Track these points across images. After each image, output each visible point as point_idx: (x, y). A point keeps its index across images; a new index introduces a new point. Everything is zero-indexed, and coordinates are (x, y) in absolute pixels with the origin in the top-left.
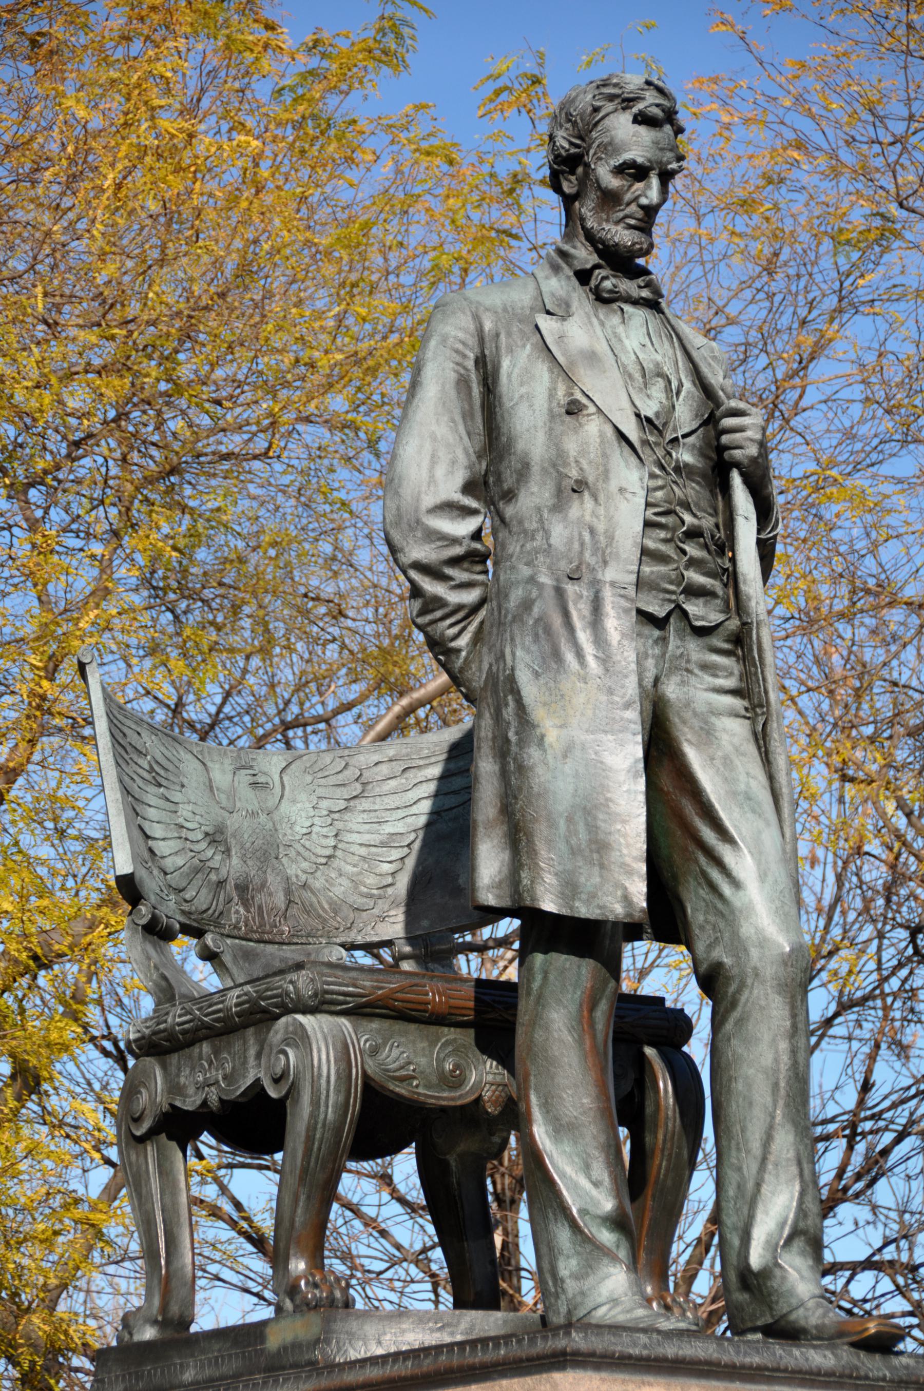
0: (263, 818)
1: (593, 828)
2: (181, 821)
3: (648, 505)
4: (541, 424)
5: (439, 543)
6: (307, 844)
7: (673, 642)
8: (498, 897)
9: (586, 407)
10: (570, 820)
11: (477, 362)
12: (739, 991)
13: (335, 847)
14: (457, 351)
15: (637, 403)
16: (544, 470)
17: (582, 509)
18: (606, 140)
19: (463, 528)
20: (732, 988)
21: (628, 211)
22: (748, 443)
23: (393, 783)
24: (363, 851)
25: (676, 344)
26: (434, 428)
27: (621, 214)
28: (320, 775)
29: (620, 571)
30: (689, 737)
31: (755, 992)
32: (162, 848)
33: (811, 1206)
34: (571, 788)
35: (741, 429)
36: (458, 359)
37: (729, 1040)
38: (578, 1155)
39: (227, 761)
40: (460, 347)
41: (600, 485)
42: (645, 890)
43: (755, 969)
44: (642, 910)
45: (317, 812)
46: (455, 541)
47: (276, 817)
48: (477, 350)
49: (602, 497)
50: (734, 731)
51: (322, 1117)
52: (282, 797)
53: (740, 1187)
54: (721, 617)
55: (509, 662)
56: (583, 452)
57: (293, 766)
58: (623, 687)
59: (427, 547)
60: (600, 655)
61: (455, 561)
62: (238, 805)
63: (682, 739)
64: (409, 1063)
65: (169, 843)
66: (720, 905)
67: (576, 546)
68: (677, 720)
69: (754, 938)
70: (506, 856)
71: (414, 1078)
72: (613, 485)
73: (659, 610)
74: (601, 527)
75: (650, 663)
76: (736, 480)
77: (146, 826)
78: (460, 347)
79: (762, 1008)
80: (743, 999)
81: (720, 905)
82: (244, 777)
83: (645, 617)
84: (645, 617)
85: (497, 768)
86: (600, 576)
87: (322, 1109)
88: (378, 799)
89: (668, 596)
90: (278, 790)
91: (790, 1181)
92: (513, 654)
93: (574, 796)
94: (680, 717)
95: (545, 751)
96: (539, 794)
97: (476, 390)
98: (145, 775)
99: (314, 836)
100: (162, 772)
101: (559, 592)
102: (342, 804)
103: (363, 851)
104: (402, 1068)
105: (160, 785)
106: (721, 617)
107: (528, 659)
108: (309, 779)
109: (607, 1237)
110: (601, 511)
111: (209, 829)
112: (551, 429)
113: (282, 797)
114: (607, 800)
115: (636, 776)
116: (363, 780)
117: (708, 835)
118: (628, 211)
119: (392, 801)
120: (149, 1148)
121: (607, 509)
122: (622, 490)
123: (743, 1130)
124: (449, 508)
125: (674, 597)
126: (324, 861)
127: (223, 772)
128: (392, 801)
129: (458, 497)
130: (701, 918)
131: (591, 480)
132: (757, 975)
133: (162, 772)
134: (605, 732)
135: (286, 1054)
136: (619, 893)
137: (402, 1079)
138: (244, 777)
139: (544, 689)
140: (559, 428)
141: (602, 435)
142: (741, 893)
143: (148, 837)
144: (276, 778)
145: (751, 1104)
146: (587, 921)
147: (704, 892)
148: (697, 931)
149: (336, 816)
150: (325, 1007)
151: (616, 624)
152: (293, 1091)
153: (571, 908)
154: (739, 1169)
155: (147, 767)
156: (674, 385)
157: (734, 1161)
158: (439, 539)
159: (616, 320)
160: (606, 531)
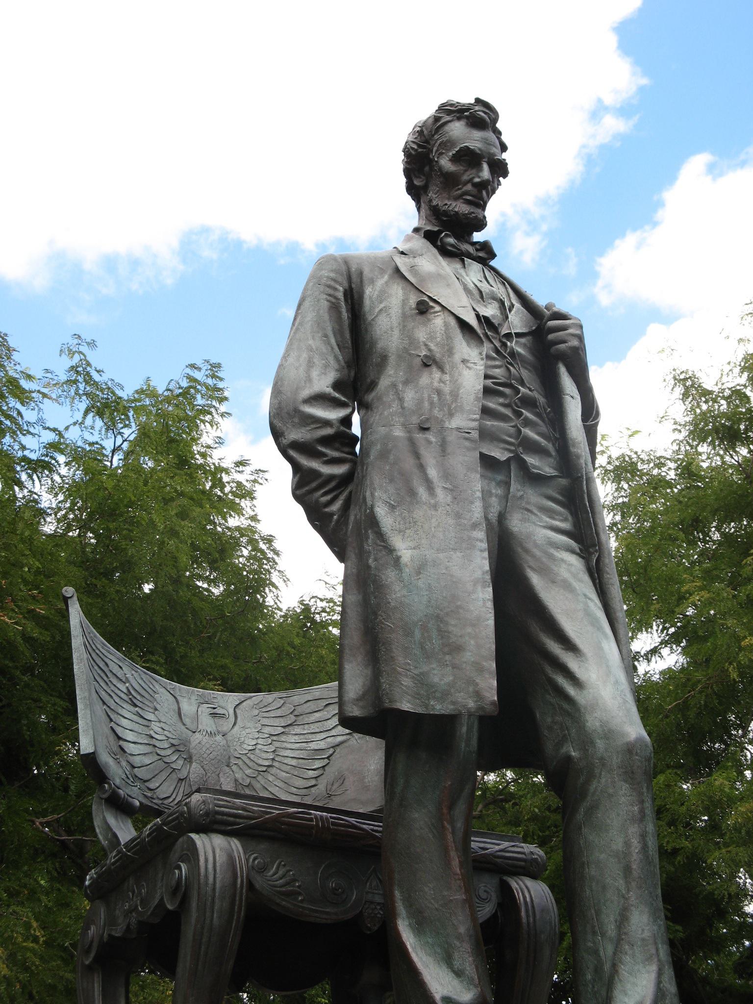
0: (219, 738)
1: (443, 634)
2: (152, 733)
3: (487, 377)
4: (395, 324)
5: (313, 426)
6: (252, 757)
7: (514, 486)
8: (363, 707)
9: (432, 307)
10: (424, 628)
11: (345, 294)
12: (588, 782)
13: (273, 759)
14: (329, 286)
15: (478, 310)
16: (399, 357)
17: (431, 379)
18: (445, 139)
19: (334, 415)
20: (582, 779)
21: (465, 188)
22: (570, 338)
23: (317, 715)
24: (294, 762)
25: (508, 286)
26: (311, 342)
27: (459, 192)
28: (264, 710)
29: (466, 419)
31: (603, 780)
32: (130, 748)
33: (667, 985)
34: (425, 599)
36: (331, 292)
37: (580, 828)
39: (194, 698)
40: (332, 283)
41: (445, 360)
42: (495, 683)
43: (602, 759)
44: (493, 703)
45: (261, 735)
46: (327, 423)
47: (229, 737)
48: (346, 285)
49: (447, 367)
50: (571, 565)
51: (208, 921)
52: (235, 724)
53: (598, 970)
54: (553, 473)
55: (369, 503)
56: (432, 337)
57: (244, 704)
58: (470, 511)
59: (303, 430)
60: (448, 486)
61: (326, 441)
62: (200, 727)
63: (525, 566)
64: (295, 880)
65: (139, 746)
66: (566, 706)
67: (426, 404)
68: (520, 550)
69: (600, 730)
70: (369, 672)
71: (300, 894)
72: (457, 358)
73: (501, 455)
74: (447, 389)
75: (494, 501)
77: (119, 730)
78: (332, 283)
79: (610, 796)
80: (592, 789)
81: (566, 706)
83: (487, 462)
84: (487, 462)
85: (360, 597)
86: (447, 425)
87: (208, 914)
88: (306, 726)
89: (508, 447)
90: (232, 719)
91: (648, 959)
92: (372, 495)
93: (427, 607)
95: (401, 570)
96: (395, 608)
97: (345, 315)
98: (123, 695)
99: (257, 751)
100: (138, 697)
101: (412, 442)
102: (281, 730)
103: (294, 762)
104: (287, 884)
105: (135, 706)
106: (553, 473)
107: (385, 496)
108: (256, 712)
110: (447, 377)
111: (174, 742)
112: (404, 326)
113: (235, 724)
114: (458, 607)
116: (296, 713)
117: (555, 648)
118: (465, 188)
119: (314, 728)
120: (96, 979)
121: (452, 376)
122: (464, 361)
123: (598, 913)
124: (319, 398)
125: (513, 448)
126: (264, 769)
127: (190, 704)
128: (314, 728)
129: (329, 390)
130: (549, 720)
131: (438, 356)
132: (603, 765)
133: (138, 697)
134: (454, 550)
135: (179, 868)
136: (471, 689)
137: (288, 894)
138: (205, 709)
139: (399, 519)
140: (410, 325)
141: (446, 325)
142: (585, 692)
143: (119, 738)
144: (231, 711)
145: (604, 888)
146: (443, 716)
147: (552, 699)
148: (546, 733)
149: (274, 738)
150: (216, 827)
151: (464, 460)
152: (184, 901)
153: (426, 706)
154: (596, 952)
155: (125, 690)
156: (507, 304)
157: (590, 944)
158: (313, 423)
159: (458, 266)
160: (451, 392)
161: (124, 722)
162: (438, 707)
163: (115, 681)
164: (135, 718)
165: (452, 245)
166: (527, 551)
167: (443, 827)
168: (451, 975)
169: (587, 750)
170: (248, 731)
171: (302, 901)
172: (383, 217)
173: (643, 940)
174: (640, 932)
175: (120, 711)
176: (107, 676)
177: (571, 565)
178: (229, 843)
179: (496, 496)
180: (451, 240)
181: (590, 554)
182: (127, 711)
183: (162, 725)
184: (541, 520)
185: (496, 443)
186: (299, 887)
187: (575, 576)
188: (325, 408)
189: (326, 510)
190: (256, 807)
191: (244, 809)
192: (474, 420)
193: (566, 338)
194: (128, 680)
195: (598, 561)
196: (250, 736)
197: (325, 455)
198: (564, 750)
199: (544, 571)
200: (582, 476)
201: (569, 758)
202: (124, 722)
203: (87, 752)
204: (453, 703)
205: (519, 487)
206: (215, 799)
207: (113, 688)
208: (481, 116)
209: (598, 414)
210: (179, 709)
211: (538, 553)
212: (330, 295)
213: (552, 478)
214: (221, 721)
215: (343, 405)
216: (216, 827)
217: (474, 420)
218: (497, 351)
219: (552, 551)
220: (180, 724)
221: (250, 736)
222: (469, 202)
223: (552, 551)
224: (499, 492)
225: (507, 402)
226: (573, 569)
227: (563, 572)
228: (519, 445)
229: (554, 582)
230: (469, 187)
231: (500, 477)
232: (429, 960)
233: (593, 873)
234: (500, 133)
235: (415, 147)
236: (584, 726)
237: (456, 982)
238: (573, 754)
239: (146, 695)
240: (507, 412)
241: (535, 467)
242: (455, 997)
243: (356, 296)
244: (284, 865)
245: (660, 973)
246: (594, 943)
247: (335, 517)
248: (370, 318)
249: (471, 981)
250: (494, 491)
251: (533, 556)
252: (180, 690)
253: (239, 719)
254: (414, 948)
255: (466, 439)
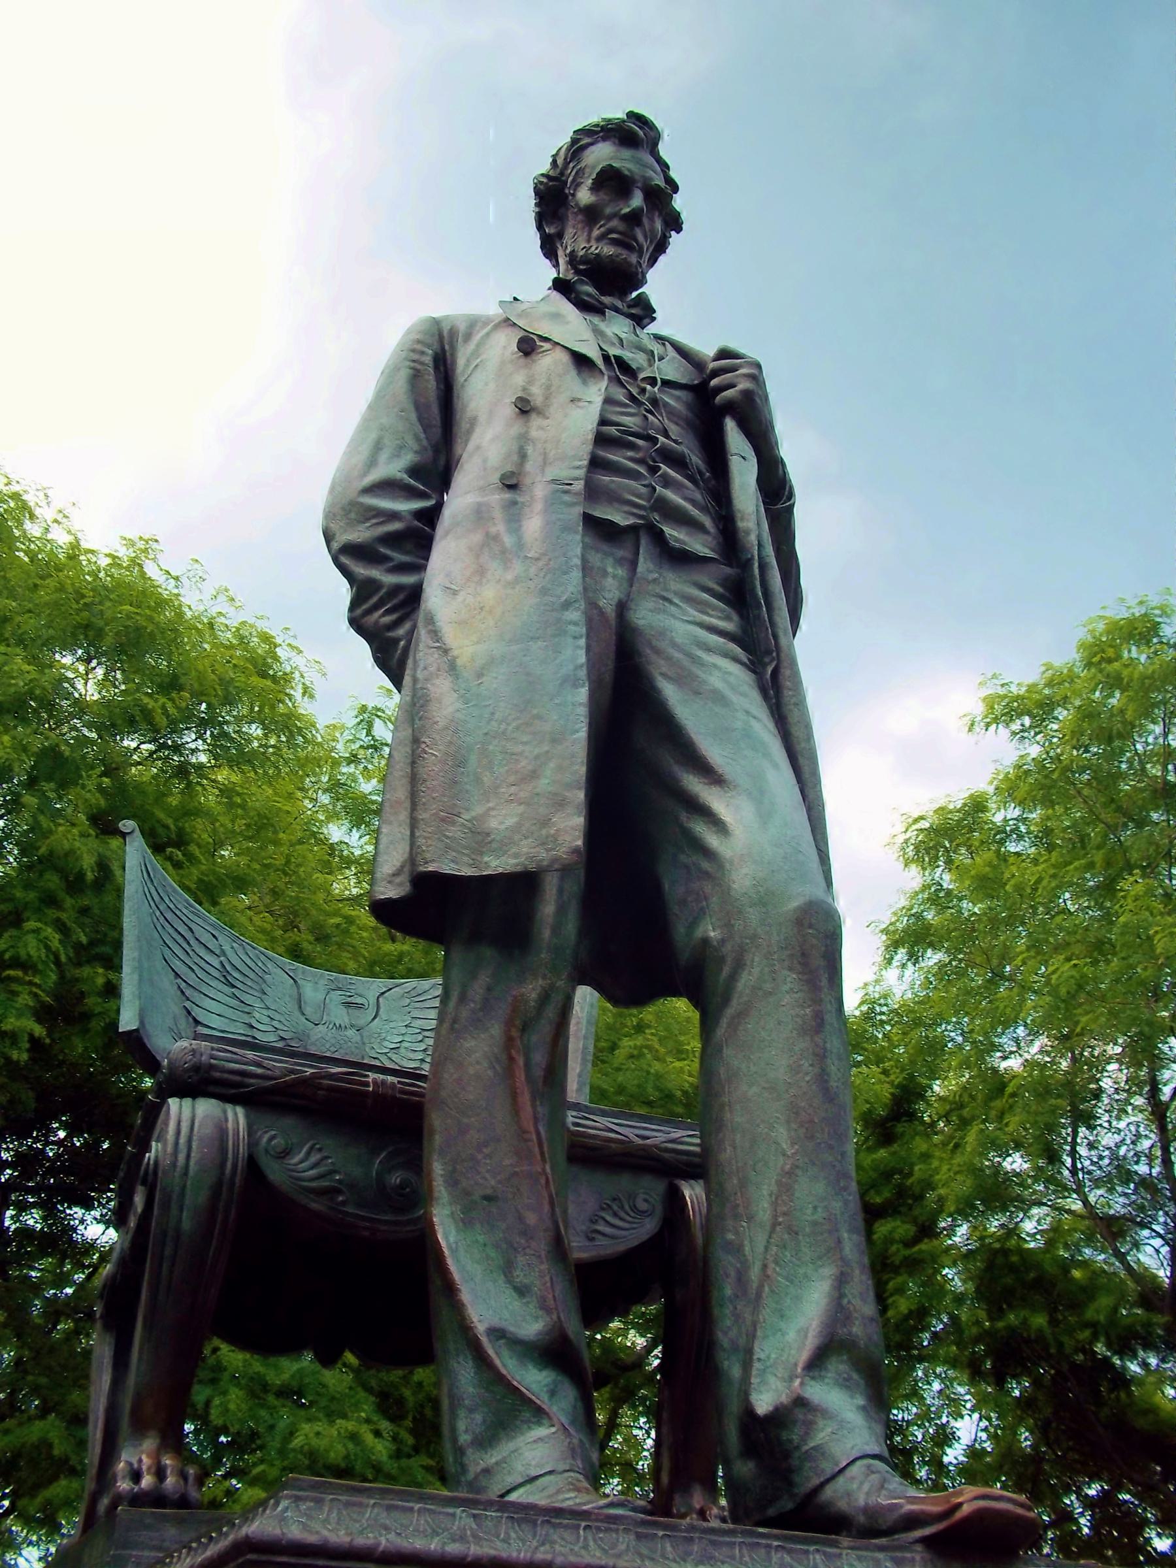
6: (394, 1057)
12: (733, 977)
20: (726, 971)
30: (664, 670)
33: (857, 1302)
35: (733, 369)
37: (720, 1051)
38: (497, 1246)
45: (410, 1030)
46: (394, 516)
48: (436, 346)
54: (711, 554)
59: (361, 527)
61: (391, 539)
73: (620, 518)
76: (730, 425)
77: (197, 1013)
81: (824, 982)
82: (336, 996)
89: (635, 511)
94: (653, 648)
98: (216, 974)
99: (402, 1050)
104: (321, 1177)
105: (234, 986)
109: (534, 1380)
115: (576, 685)
123: (743, 1184)
125: (642, 513)
127: (316, 990)
144: (373, 1001)
148: (676, 909)
150: (211, 1089)
157: (730, 1236)
158: (374, 517)
161: (207, 1003)
162: (494, 864)
163: (202, 952)
164: (234, 1002)
165: (589, 295)
166: (658, 652)
167: (511, 1059)
168: (510, 1292)
169: (733, 926)
170: (392, 1025)
171: (343, 1203)
172: (507, 274)
173: (815, 1224)
174: (809, 1211)
175: (205, 989)
176: (188, 943)
177: (730, 673)
178: (225, 1112)
179: (614, 577)
180: (589, 289)
181: (765, 665)
182: (217, 990)
183: (270, 1013)
184: (685, 613)
185: (616, 505)
186: (339, 1181)
187: (733, 688)
188: (394, 498)
189: (390, 634)
190: (278, 1065)
191: (259, 1065)
192: (578, 468)
193: (736, 380)
194: (224, 953)
195: (775, 672)
196: (395, 1032)
197: (387, 559)
198: (699, 933)
199: (684, 679)
200: (752, 558)
201: (706, 941)
202: (207, 1003)
203: (129, 1028)
204: (516, 856)
205: (651, 566)
206: (213, 1049)
207: (197, 960)
208: (634, 133)
209: (791, 495)
210: (300, 995)
211: (677, 655)
212: (414, 361)
213: (705, 560)
214: (356, 1012)
215: (422, 495)
216: (211, 1089)
217: (578, 468)
218: (632, 398)
219: (700, 653)
220: (297, 1013)
221: (395, 1032)
222: (615, 242)
223: (700, 653)
224: (621, 572)
225: (639, 455)
226: (732, 679)
227: (715, 681)
228: (654, 508)
229: (697, 693)
230: (614, 223)
231: (620, 553)
232: (477, 1270)
233: (738, 1119)
234: (668, 168)
235: (545, 180)
236: (729, 888)
237: (516, 1304)
238: (712, 934)
239: (252, 975)
240: (642, 470)
241: (677, 540)
242: (512, 1329)
243: (449, 362)
244: (320, 1150)
245: (841, 1281)
246: (737, 1233)
247: (402, 643)
248: (461, 379)
249: (543, 1306)
250: (610, 570)
251: (669, 659)
252: (303, 973)
253: (381, 1010)
254: (454, 1251)
255: (566, 492)
